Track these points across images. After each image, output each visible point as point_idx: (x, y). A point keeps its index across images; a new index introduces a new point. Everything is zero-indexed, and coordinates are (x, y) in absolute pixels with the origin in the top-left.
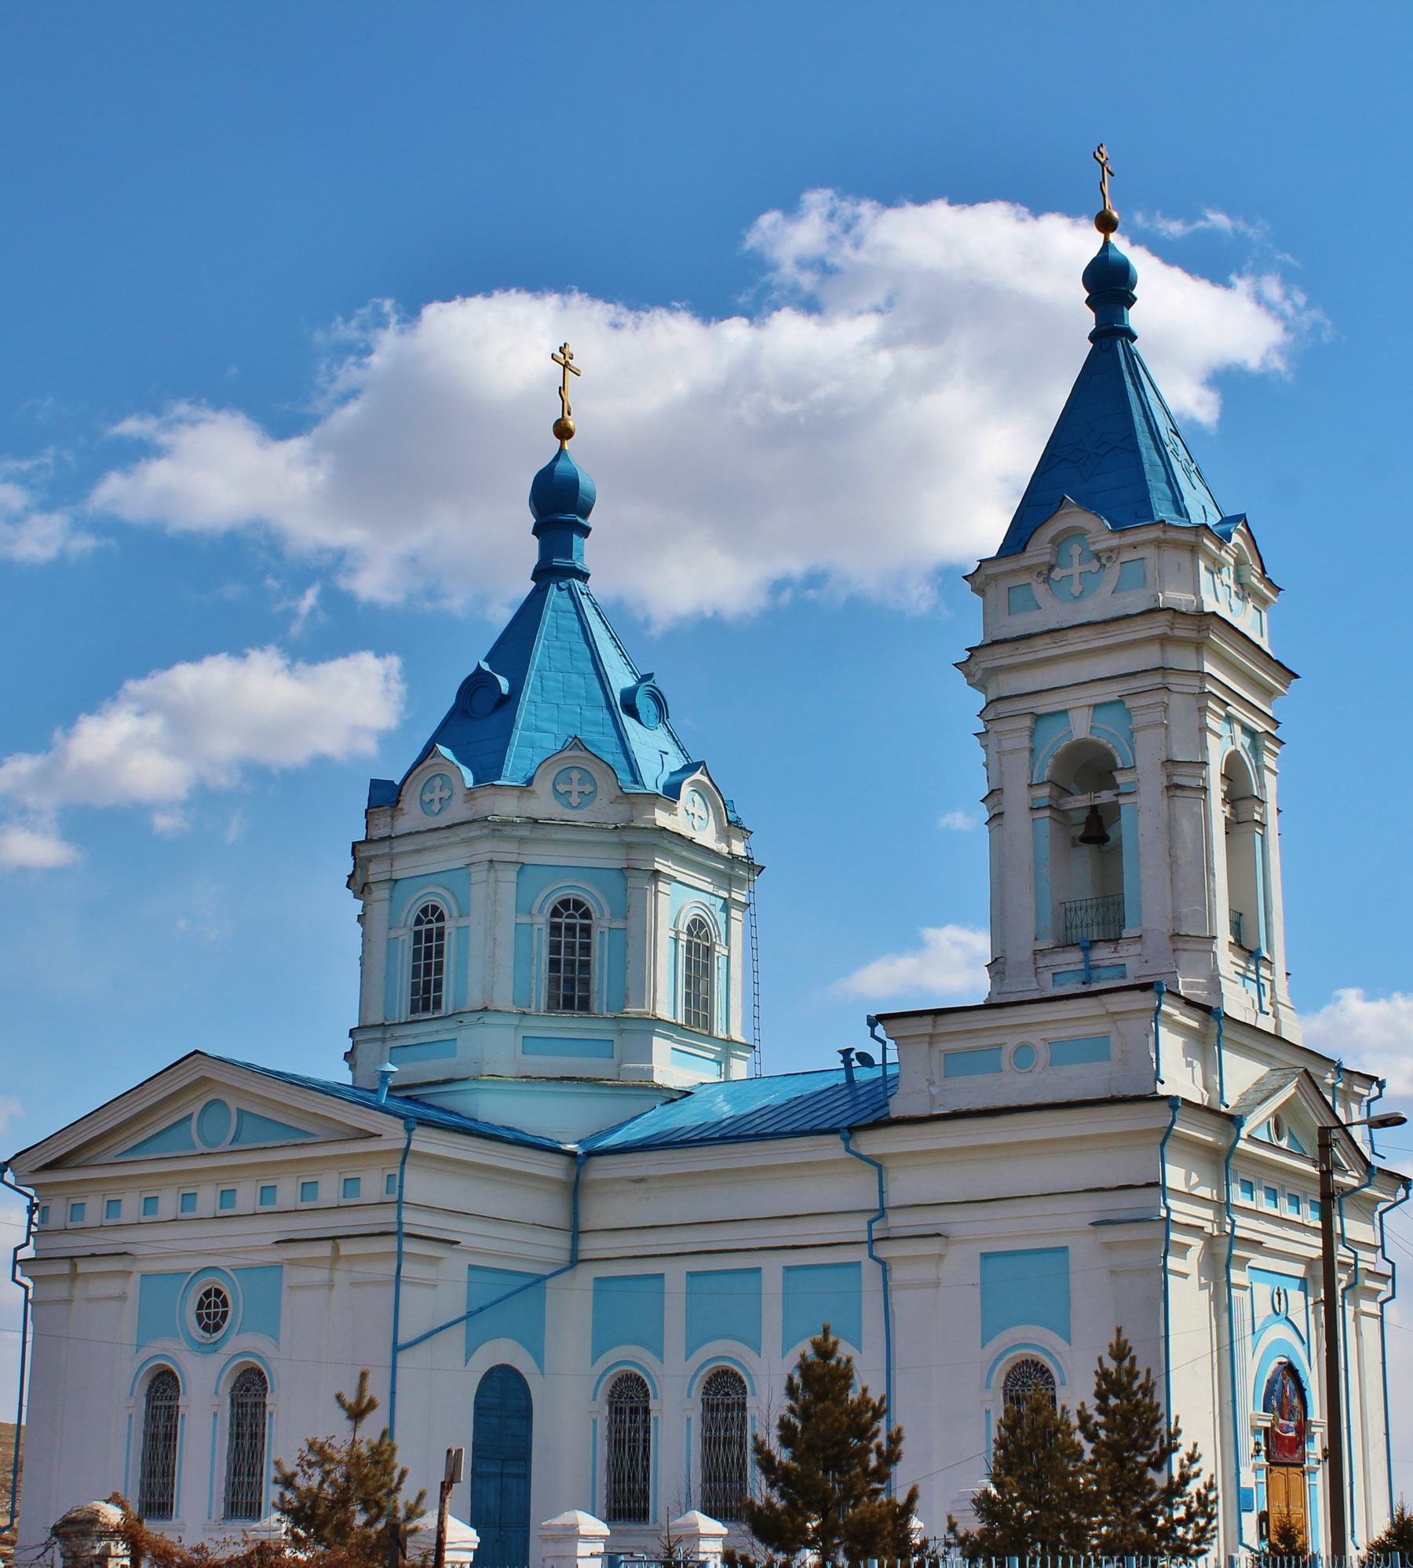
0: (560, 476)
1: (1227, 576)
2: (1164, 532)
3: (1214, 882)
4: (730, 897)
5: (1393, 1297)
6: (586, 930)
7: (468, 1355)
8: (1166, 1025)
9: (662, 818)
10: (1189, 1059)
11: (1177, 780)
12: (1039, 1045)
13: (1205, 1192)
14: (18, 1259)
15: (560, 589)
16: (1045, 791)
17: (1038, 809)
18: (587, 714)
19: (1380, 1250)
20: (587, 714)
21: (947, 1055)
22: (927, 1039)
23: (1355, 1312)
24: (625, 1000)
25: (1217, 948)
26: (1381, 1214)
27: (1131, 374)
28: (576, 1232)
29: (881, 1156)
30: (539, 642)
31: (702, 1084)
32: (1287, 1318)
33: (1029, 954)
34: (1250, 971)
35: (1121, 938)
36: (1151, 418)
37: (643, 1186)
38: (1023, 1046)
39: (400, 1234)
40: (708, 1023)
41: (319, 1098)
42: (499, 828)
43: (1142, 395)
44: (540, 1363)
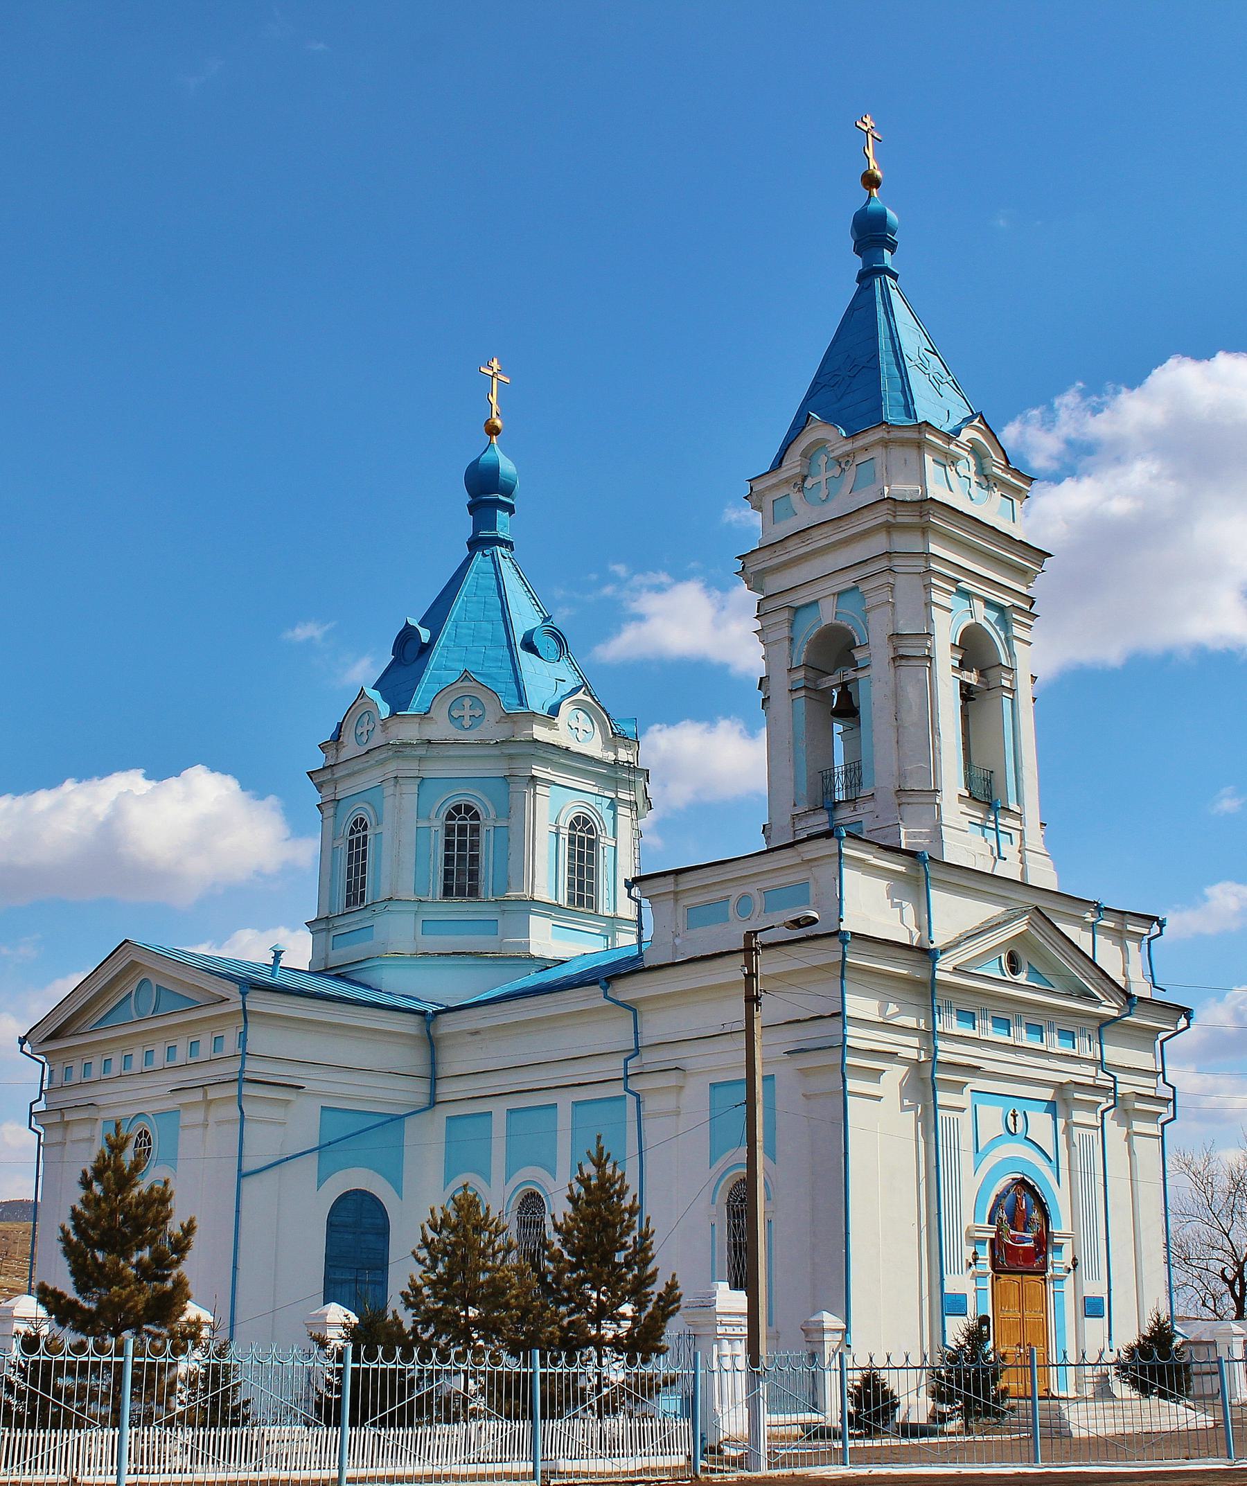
0: (484, 464)
1: (967, 466)
2: (888, 432)
3: (939, 741)
4: (617, 796)
5: (1174, 1118)
6: (476, 830)
7: (320, 1182)
8: (850, 867)
9: (540, 733)
10: (896, 900)
11: (902, 651)
12: (756, 894)
13: (910, 1022)
14: (33, 1111)
15: (484, 555)
16: (801, 674)
17: (795, 690)
18: (490, 653)
19: (1161, 1075)
20: (490, 653)
21: (689, 909)
22: (672, 896)
23: (1128, 1133)
24: (508, 886)
25: (941, 800)
26: (1162, 1042)
27: (884, 304)
28: (434, 1079)
29: (631, 1001)
30: (459, 598)
31: (585, 954)
32: (1026, 1138)
33: (787, 820)
34: (990, 821)
35: (856, 798)
36: (896, 339)
37: (477, 1037)
38: (744, 896)
39: (242, 1080)
40: (592, 903)
41: (485, 997)
42: (401, 749)
43: (892, 320)
44: (399, 1191)
